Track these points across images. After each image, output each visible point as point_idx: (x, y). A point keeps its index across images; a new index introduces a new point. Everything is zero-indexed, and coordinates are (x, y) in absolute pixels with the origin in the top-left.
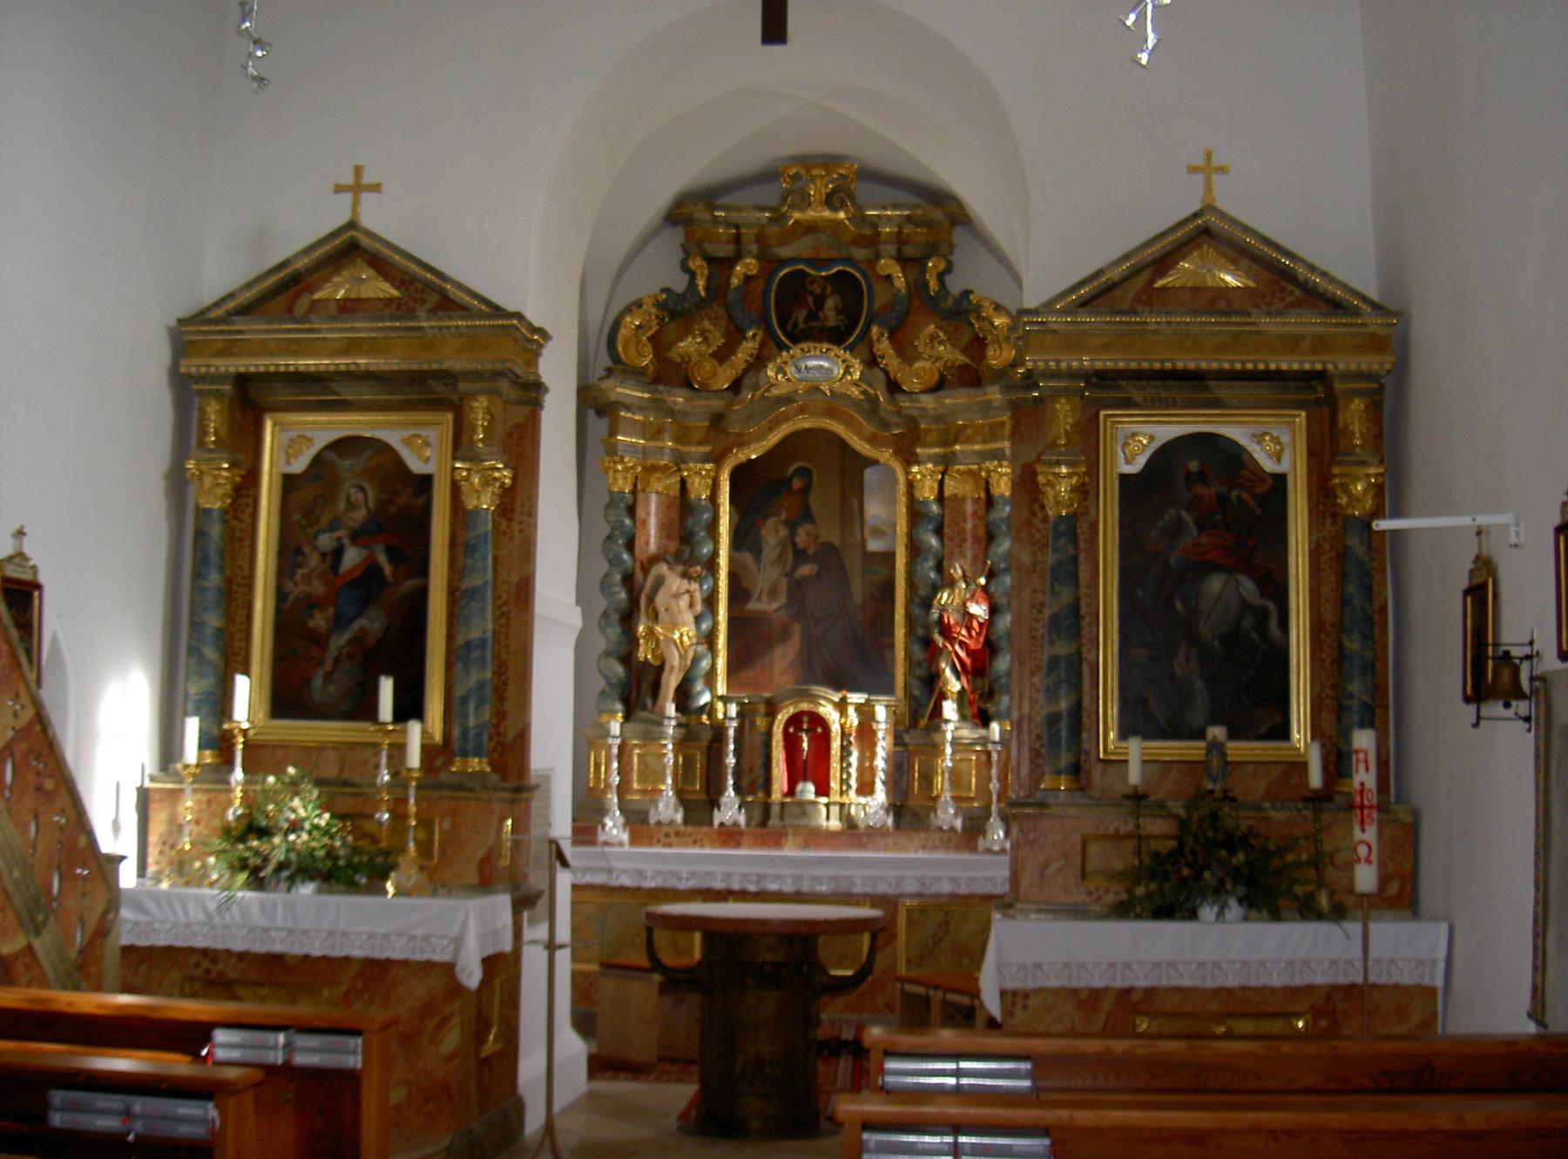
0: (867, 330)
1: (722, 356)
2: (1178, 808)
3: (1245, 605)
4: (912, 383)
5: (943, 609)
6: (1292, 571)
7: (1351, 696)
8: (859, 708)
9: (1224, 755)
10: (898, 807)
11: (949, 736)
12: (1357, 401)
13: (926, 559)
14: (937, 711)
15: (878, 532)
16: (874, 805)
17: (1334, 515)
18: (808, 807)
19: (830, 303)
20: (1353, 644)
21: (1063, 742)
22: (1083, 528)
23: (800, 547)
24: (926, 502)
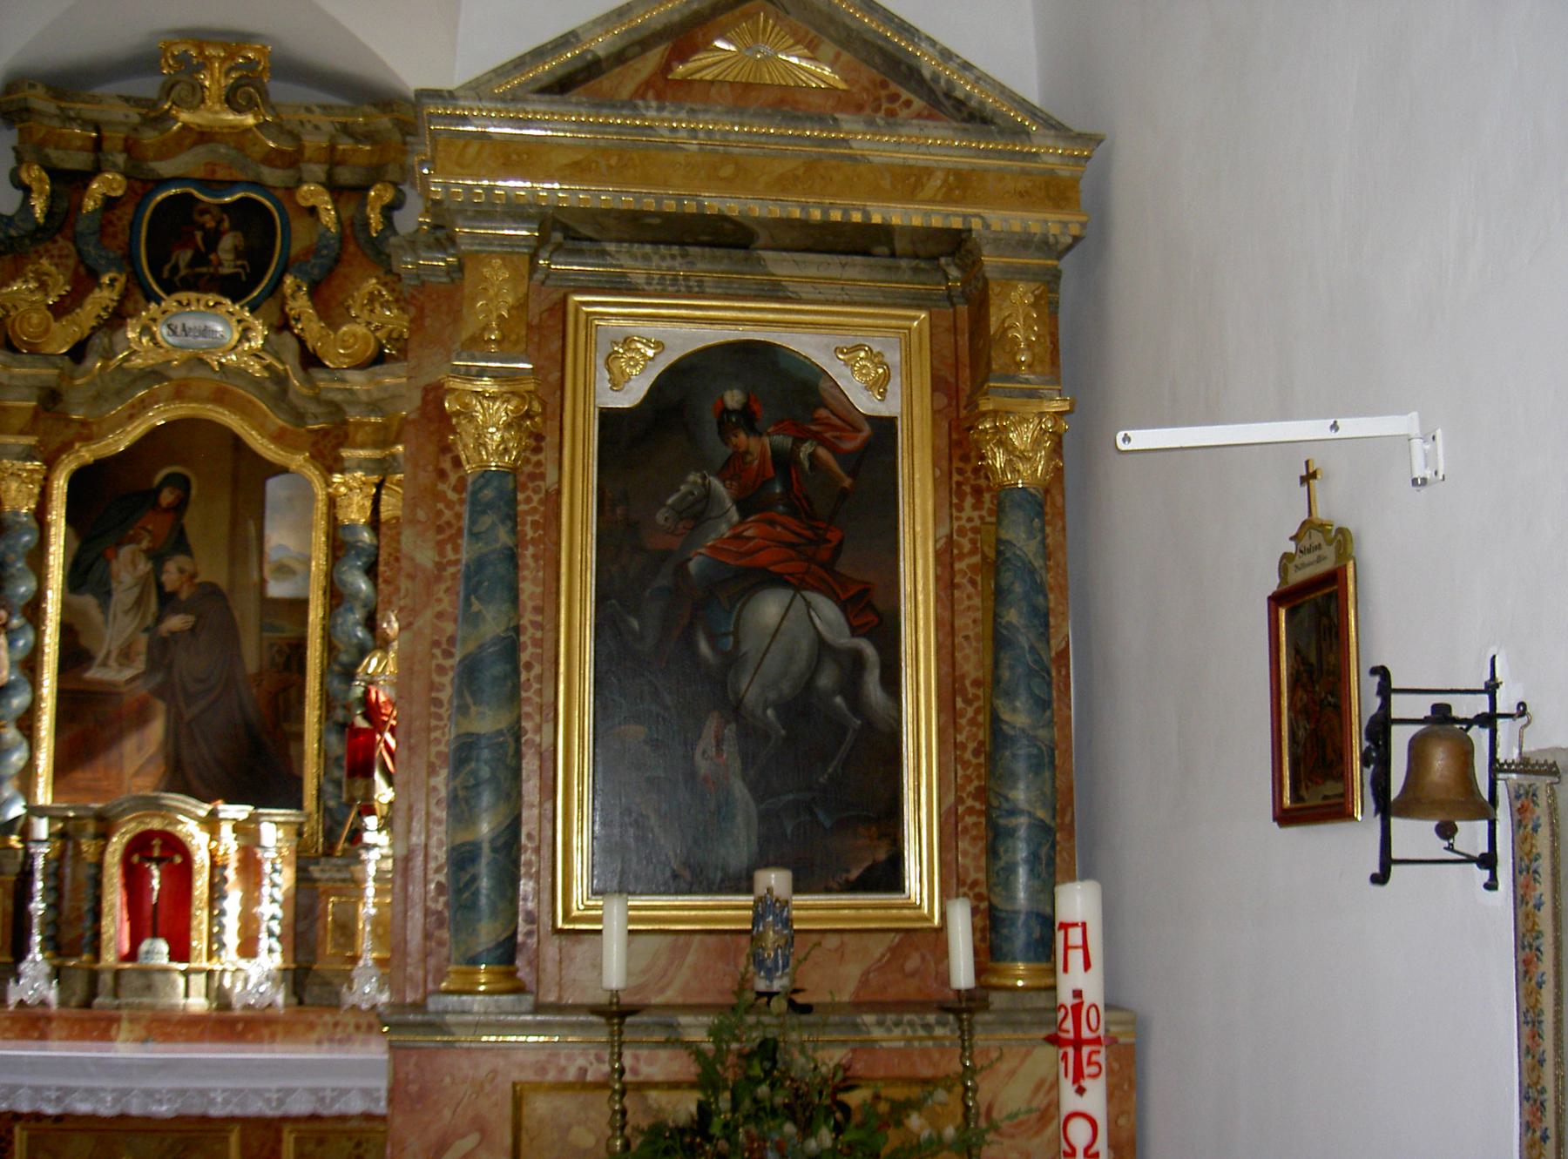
0: (278, 282)
1: (60, 310)
2: (696, 1029)
3: (822, 648)
4: (336, 354)
5: (371, 681)
6: (906, 587)
7: (1013, 812)
8: (238, 827)
9: (787, 922)
10: (302, 977)
11: (371, 870)
12: (1021, 287)
13: (351, 610)
14: (356, 835)
15: (283, 570)
16: (257, 974)
17: (978, 492)
18: (158, 978)
19: (228, 242)
20: (1018, 717)
21: (483, 901)
22: (530, 501)
23: (169, 588)
24: (352, 527)
